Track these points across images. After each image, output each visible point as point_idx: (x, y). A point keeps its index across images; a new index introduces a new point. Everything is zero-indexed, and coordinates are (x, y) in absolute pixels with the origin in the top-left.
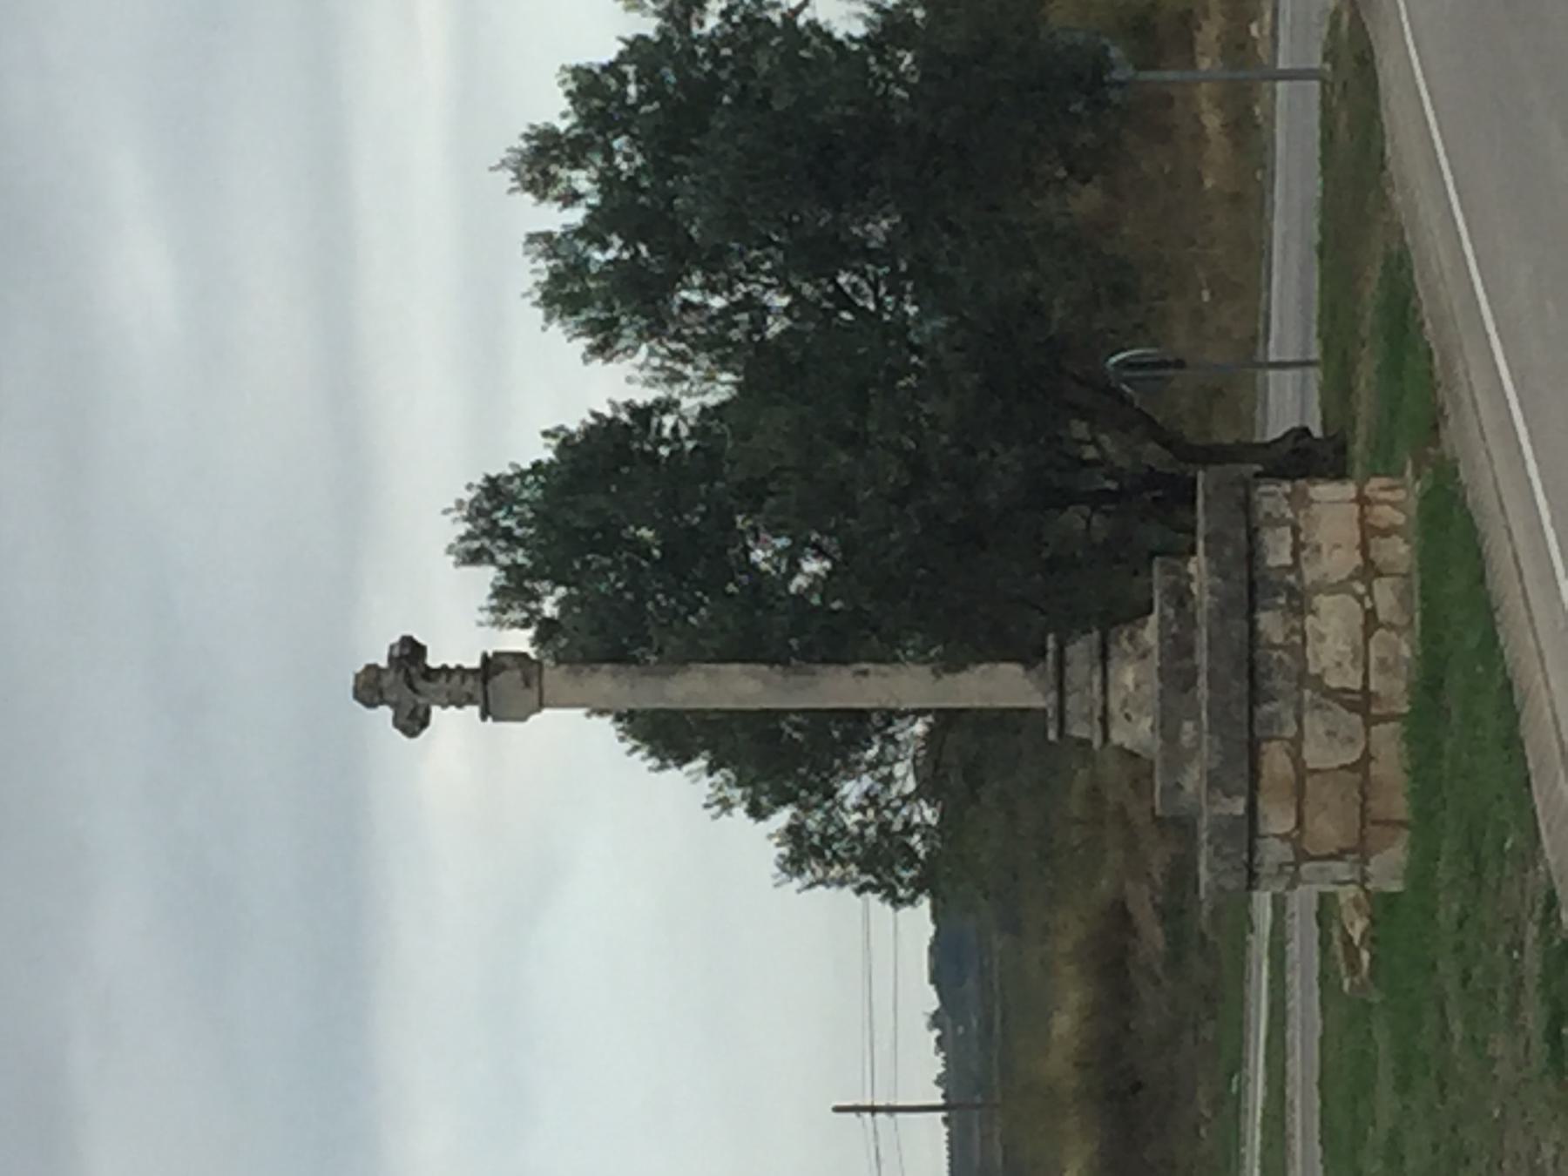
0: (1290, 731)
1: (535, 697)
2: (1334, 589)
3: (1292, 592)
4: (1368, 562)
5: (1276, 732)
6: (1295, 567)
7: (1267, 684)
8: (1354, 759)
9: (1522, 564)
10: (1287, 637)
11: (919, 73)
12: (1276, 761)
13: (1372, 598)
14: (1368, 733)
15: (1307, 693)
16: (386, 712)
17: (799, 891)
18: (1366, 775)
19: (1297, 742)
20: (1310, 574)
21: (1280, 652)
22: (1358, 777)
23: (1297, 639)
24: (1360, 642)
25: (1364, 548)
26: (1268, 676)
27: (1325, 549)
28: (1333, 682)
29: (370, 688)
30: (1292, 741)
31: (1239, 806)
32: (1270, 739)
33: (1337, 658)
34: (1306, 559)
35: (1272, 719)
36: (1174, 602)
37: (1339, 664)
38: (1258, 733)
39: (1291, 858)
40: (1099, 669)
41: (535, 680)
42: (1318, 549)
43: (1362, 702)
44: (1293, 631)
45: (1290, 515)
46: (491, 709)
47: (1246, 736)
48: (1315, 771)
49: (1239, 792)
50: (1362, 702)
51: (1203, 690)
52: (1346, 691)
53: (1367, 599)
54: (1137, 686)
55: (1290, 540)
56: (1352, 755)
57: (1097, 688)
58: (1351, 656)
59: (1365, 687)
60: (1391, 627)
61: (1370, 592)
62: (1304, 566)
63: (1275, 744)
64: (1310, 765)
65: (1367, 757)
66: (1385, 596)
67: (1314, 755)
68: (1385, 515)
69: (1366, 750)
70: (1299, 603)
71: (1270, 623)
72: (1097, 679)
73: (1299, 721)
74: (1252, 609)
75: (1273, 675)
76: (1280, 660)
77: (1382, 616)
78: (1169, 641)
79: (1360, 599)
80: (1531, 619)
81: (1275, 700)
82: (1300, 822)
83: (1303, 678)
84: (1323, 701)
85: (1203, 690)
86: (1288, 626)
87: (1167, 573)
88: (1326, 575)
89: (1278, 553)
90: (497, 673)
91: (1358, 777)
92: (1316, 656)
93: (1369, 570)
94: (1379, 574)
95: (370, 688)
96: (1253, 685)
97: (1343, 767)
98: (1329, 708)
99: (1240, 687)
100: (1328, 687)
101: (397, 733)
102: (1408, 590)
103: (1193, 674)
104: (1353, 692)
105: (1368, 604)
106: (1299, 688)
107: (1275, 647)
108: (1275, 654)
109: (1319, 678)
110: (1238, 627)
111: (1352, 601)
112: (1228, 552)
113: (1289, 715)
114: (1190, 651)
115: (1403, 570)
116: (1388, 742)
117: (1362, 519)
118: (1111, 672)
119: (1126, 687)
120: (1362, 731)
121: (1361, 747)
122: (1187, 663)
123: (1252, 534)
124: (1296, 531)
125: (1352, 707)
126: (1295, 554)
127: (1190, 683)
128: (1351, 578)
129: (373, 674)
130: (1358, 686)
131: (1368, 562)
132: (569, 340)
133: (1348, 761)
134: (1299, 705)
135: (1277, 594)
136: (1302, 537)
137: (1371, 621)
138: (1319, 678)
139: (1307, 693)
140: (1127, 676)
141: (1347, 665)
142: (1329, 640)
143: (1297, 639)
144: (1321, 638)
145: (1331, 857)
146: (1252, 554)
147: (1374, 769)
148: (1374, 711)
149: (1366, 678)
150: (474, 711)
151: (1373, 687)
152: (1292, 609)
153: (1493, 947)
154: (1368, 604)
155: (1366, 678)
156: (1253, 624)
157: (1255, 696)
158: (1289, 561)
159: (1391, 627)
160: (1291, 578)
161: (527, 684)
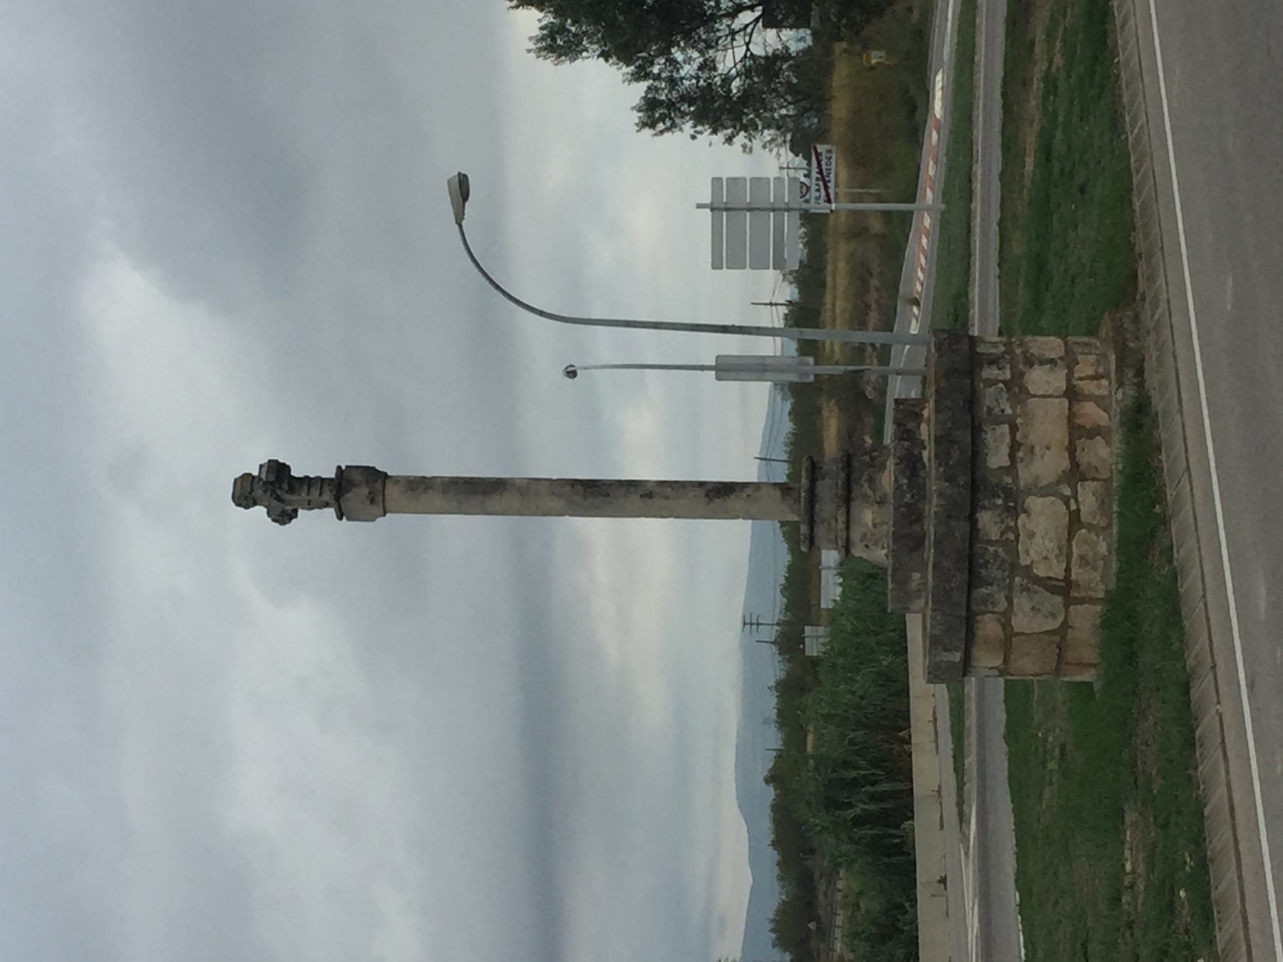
0: (1003, 605)
1: (382, 510)
2: (1044, 492)
3: (1009, 494)
4: (1075, 464)
5: (990, 607)
6: (1011, 469)
8: (1056, 627)
9: (1203, 553)
10: (1002, 534)
11: (668, 87)
12: (988, 627)
13: (1076, 501)
16: (260, 511)
18: (1063, 638)
22: (1058, 638)
23: (1011, 536)
24: (1064, 542)
25: (1072, 450)
27: (1037, 449)
28: (1040, 571)
29: (246, 491)
30: (1003, 614)
32: (984, 613)
33: (1044, 553)
34: (1022, 460)
35: (986, 600)
36: (908, 473)
37: (1046, 558)
38: (974, 608)
40: (843, 509)
42: (1032, 449)
43: (1065, 588)
44: (1008, 528)
45: (1009, 411)
46: (344, 512)
48: (1017, 634)
49: (957, 649)
50: (1065, 588)
51: (930, 554)
53: (1072, 501)
54: (875, 526)
55: (1008, 439)
56: (1054, 624)
57: (841, 526)
58: (1057, 552)
59: (1067, 579)
60: (1090, 527)
63: (988, 617)
64: (1016, 630)
65: (1065, 625)
66: (1088, 498)
67: (1021, 622)
68: (1091, 413)
69: (1065, 621)
70: (1014, 505)
71: (988, 521)
72: (841, 518)
74: (974, 508)
75: (989, 566)
76: (996, 555)
77: (1084, 517)
78: (903, 509)
79: (1067, 504)
80: (1214, 667)
81: (991, 585)
82: (1005, 662)
83: (1014, 567)
85: (930, 554)
86: (1004, 526)
87: (902, 439)
88: (1037, 478)
89: (997, 458)
91: (1058, 638)
92: (1027, 552)
93: (1075, 474)
94: (1084, 479)
95: (246, 491)
96: (971, 571)
97: (1046, 632)
98: (1036, 592)
99: (960, 578)
100: (1037, 576)
101: (288, 463)
106: (1012, 576)
107: (990, 542)
108: (991, 549)
109: (1028, 568)
110: (961, 528)
111: (1059, 502)
112: (955, 453)
113: (1001, 597)
115: (1105, 475)
116: (1085, 619)
117: (1071, 416)
118: (853, 512)
119: (867, 525)
120: (1063, 610)
121: (1061, 619)
122: (916, 528)
123: (976, 431)
124: (1014, 428)
125: (1054, 590)
126: (1012, 456)
127: (917, 543)
128: (1058, 482)
129: (247, 485)
130: (1061, 575)
131: (1075, 464)
132: (339, 468)
133: (1049, 628)
134: (1010, 588)
135: (995, 496)
136: (1019, 436)
137: (1075, 521)
138: (1028, 568)
140: (867, 516)
141: (1052, 557)
142: (1038, 539)
143: (1011, 536)
144: (1032, 535)
146: (975, 454)
147: (1070, 634)
148: (1074, 594)
149: (1068, 570)
150: (330, 512)
151: (1073, 577)
152: (1008, 509)
154: (1073, 507)
155: (1068, 570)
156: (973, 520)
157: (973, 580)
158: (1005, 462)
159: (1090, 527)
160: (1008, 480)
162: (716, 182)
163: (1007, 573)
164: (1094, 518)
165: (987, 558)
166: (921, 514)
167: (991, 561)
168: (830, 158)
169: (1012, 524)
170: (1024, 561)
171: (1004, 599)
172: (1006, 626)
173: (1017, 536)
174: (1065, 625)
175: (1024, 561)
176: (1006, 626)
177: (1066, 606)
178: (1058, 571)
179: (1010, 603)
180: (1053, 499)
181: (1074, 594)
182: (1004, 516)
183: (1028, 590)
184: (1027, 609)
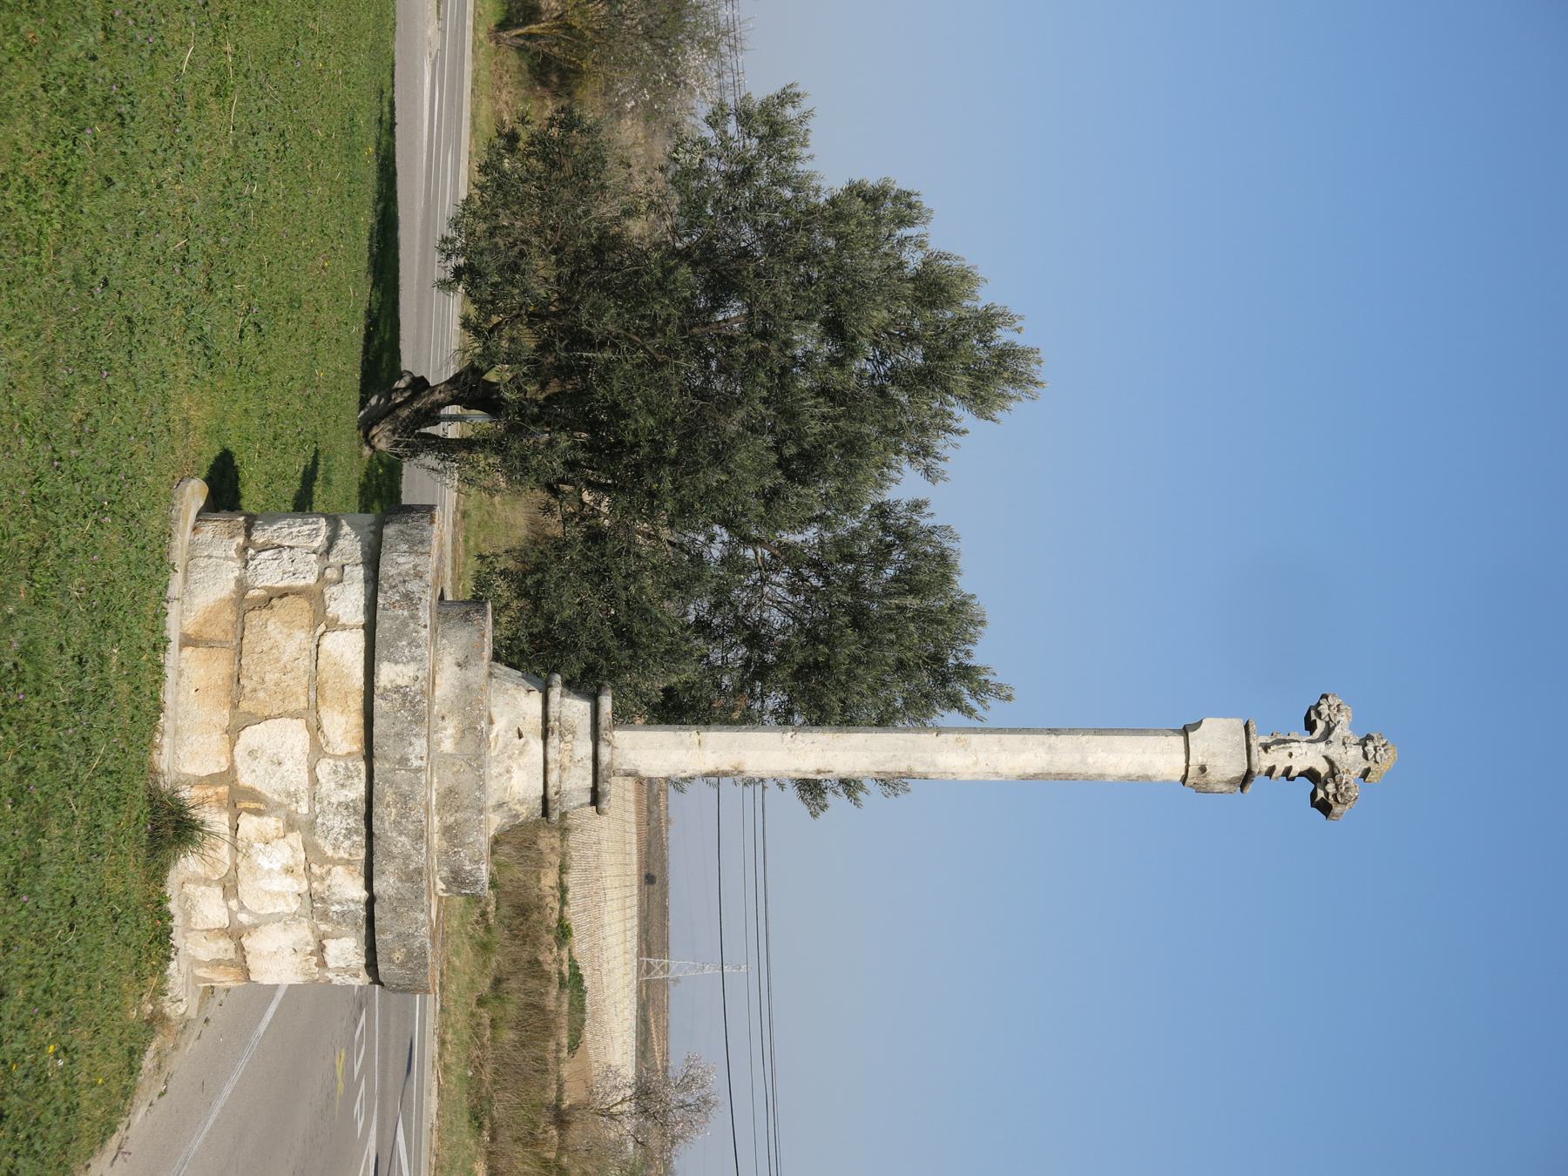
7: (351, 822)
12: (343, 728)
14: (233, 761)
15: (303, 809)
17: (945, 459)
19: (318, 749)
20: (303, 933)
21: (336, 856)
26: (349, 833)
28: (271, 824)
31: (387, 674)
39: (330, 591)
40: (551, 791)
41: (1193, 770)
47: (377, 765)
52: (258, 813)
56: (251, 736)
58: (252, 851)
61: (232, 915)
62: (310, 938)
64: (301, 723)
65: (233, 733)
69: (233, 745)
72: (553, 778)
73: (315, 781)
74: (371, 902)
84: (286, 801)
86: (327, 882)
90: (1236, 778)
102: (188, 916)
103: (442, 806)
104: (250, 811)
105: (233, 903)
108: (343, 854)
113: (327, 784)
114: (447, 830)
121: (240, 749)
125: (252, 794)
126: (321, 949)
137: (230, 887)
139: (303, 809)
145: (283, 594)
153: (60, 691)
155: (235, 829)
156: (369, 885)
159: (207, 882)
160: (324, 927)
161: (1203, 769)
162: (931, 211)
163: (319, 820)
164: (204, 894)
165: (347, 843)
166: (444, 835)
167: (341, 839)
168: (662, 1060)
169: (315, 885)
170: (296, 838)
171: (322, 781)
172: (316, 729)
173: (308, 869)
174: (233, 733)
175: (296, 838)
176: (316, 729)
177: (232, 769)
178: (248, 824)
179: (312, 770)
180: (262, 912)
181: (223, 790)
182: (327, 893)
183: (289, 795)
184: (289, 765)
